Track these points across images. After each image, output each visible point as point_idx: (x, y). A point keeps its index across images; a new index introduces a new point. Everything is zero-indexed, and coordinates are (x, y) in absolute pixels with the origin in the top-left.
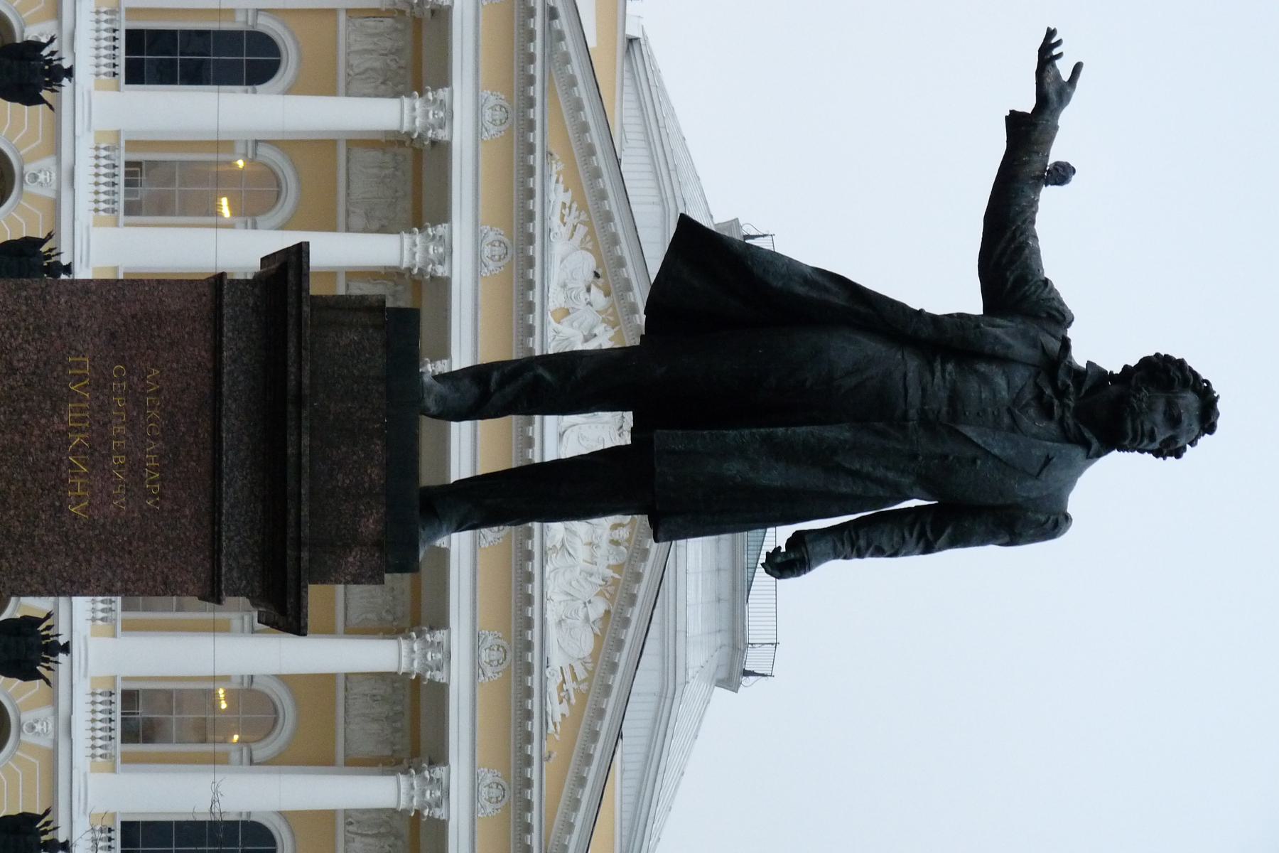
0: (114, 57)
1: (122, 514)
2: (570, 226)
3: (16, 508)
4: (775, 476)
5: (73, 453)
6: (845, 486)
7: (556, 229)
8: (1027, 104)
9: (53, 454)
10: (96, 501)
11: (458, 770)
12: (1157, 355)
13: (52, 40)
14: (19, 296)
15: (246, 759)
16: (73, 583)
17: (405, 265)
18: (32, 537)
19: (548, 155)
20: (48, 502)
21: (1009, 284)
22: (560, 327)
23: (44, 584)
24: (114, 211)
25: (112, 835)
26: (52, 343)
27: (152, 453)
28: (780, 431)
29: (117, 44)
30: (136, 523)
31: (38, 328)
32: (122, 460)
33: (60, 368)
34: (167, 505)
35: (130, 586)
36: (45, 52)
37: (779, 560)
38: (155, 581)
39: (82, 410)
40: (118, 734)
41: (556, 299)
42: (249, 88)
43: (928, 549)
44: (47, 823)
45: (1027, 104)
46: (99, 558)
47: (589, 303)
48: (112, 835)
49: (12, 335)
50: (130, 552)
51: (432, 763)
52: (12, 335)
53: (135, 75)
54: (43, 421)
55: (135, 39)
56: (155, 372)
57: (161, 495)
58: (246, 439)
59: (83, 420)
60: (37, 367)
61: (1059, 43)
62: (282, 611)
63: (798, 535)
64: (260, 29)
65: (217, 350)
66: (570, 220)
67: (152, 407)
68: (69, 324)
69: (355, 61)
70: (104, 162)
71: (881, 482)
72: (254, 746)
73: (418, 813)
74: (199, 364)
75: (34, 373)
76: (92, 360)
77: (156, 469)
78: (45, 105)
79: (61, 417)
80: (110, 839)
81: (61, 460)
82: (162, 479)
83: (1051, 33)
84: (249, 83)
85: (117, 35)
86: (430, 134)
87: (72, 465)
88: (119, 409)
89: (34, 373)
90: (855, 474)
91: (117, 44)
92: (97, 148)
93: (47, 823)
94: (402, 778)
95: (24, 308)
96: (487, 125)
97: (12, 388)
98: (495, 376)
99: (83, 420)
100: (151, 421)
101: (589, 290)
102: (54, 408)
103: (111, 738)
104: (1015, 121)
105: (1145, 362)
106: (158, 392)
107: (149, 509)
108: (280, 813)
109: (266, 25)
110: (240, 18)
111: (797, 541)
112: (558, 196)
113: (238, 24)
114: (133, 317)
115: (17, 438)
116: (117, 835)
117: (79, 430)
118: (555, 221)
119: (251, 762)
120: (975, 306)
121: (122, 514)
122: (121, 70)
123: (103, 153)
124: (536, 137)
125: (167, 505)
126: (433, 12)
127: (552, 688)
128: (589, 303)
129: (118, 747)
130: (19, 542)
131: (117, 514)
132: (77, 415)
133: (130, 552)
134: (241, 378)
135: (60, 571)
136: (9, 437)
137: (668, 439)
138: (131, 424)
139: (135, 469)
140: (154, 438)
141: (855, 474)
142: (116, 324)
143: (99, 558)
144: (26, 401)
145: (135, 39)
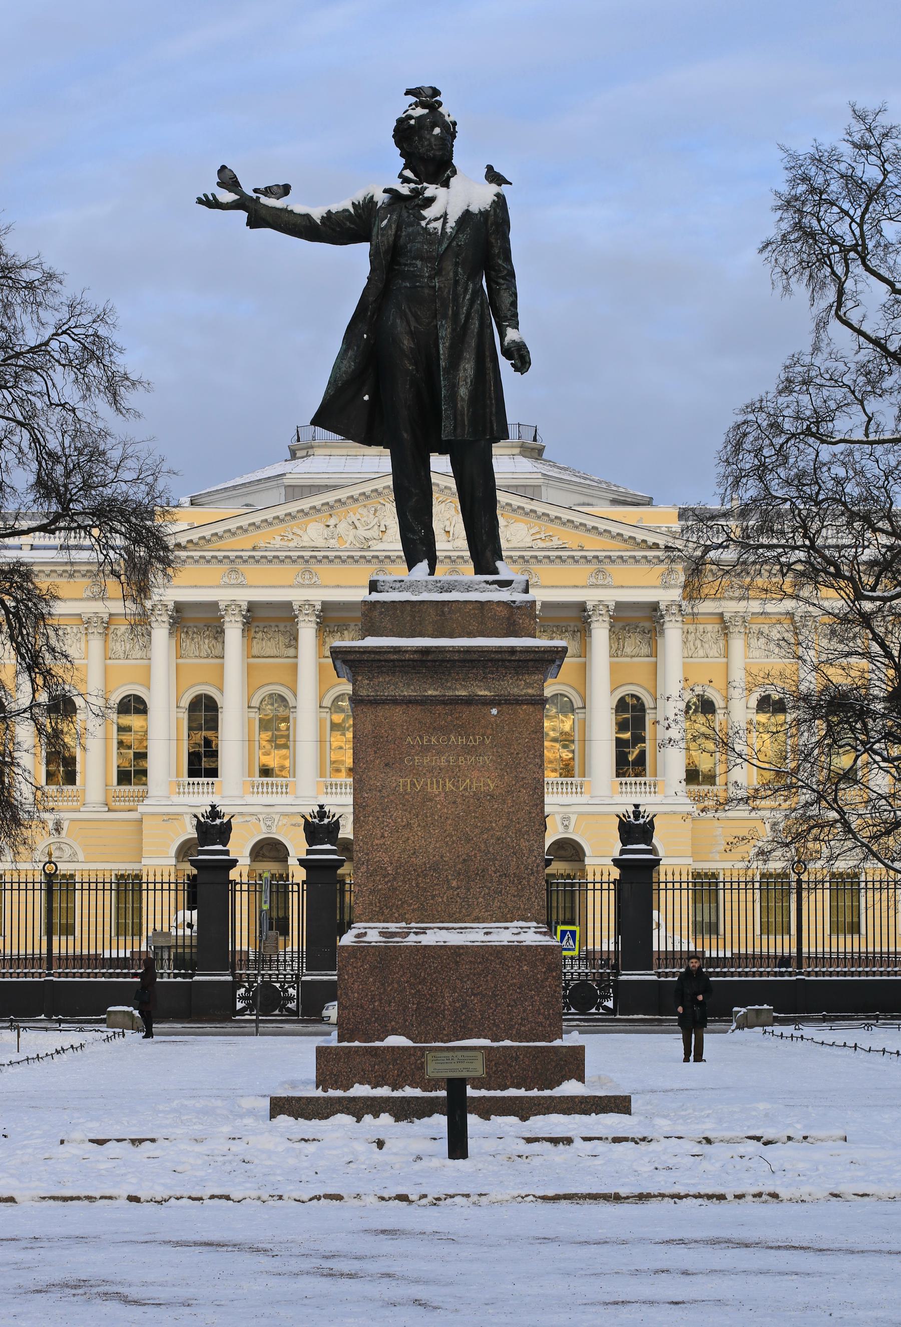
0: (203, 784)
1: (494, 758)
2: (294, 537)
3: (491, 822)
4: (468, 368)
5: (458, 788)
6: (475, 325)
7: (295, 544)
8: (243, 215)
9: (459, 800)
10: (487, 774)
11: (590, 596)
12: (393, 136)
13: (196, 816)
14: (363, 821)
15: (583, 711)
16: (536, 788)
17: (315, 626)
18: (509, 813)
19: (254, 549)
20: (487, 803)
21: (352, 226)
22: (349, 542)
23: (537, 805)
25: (624, 782)
26: (392, 801)
27: (457, 741)
28: (443, 364)
29: (196, 783)
31: (383, 810)
32: (461, 758)
33: (407, 797)
34: (489, 731)
35: (538, 754)
36: (202, 820)
37: (519, 365)
38: (534, 739)
39: (432, 783)
40: (569, 780)
42: (220, 710)
43: (512, 274)
44: (624, 816)
45: (243, 215)
46: (521, 772)
47: (335, 526)
48: (624, 782)
49: (387, 826)
50: (517, 754)
51: (585, 610)
52: (387, 826)
53: (213, 773)
54: (439, 806)
55: (193, 773)
56: (409, 739)
57: (483, 735)
58: (449, 684)
59: (438, 782)
60: (406, 810)
61: (205, 195)
62: (553, 661)
63: (504, 354)
64: (187, 706)
65: (395, 702)
66: (290, 537)
67: (430, 741)
68: (380, 791)
69: (204, 654)
71: (472, 302)
72: (575, 707)
73: (611, 617)
74: (404, 713)
75: (410, 812)
77: (467, 739)
78: (232, 820)
79: (436, 796)
80: (626, 784)
81: (463, 795)
82: (474, 735)
83: (200, 201)
84: (217, 711)
85: (191, 782)
86: (244, 613)
87: (465, 789)
88: (431, 761)
89: (410, 812)
90: (468, 316)
91: (196, 783)
92: (253, 793)
93: (624, 816)
94: (593, 626)
95: (371, 818)
97: (419, 825)
98: (378, 606)
99: (438, 782)
100: (438, 741)
101: (328, 526)
102: (431, 800)
103: (572, 784)
104: (253, 223)
105: (398, 144)
106: (421, 738)
107: (491, 742)
108: (612, 692)
109: (185, 702)
110: (181, 715)
111: (507, 354)
112: (277, 542)
113: (185, 716)
114: (375, 752)
115: (449, 822)
116: (624, 780)
117: (444, 785)
118: (292, 544)
119: (584, 708)
120: (364, 248)
121: (494, 758)
122: (210, 780)
123: (255, 790)
124: (245, 554)
125: (489, 731)
127: (541, 544)
128: (335, 526)
129: (576, 780)
130: (511, 820)
131: (494, 762)
132: (435, 786)
133: (517, 754)
134: (412, 687)
135: (529, 796)
136: (448, 827)
137: (446, 432)
138: (440, 753)
140: (449, 739)
141: (468, 316)
142: (379, 764)
143: (521, 772)
144: (427, 817)
145: (193, 773)
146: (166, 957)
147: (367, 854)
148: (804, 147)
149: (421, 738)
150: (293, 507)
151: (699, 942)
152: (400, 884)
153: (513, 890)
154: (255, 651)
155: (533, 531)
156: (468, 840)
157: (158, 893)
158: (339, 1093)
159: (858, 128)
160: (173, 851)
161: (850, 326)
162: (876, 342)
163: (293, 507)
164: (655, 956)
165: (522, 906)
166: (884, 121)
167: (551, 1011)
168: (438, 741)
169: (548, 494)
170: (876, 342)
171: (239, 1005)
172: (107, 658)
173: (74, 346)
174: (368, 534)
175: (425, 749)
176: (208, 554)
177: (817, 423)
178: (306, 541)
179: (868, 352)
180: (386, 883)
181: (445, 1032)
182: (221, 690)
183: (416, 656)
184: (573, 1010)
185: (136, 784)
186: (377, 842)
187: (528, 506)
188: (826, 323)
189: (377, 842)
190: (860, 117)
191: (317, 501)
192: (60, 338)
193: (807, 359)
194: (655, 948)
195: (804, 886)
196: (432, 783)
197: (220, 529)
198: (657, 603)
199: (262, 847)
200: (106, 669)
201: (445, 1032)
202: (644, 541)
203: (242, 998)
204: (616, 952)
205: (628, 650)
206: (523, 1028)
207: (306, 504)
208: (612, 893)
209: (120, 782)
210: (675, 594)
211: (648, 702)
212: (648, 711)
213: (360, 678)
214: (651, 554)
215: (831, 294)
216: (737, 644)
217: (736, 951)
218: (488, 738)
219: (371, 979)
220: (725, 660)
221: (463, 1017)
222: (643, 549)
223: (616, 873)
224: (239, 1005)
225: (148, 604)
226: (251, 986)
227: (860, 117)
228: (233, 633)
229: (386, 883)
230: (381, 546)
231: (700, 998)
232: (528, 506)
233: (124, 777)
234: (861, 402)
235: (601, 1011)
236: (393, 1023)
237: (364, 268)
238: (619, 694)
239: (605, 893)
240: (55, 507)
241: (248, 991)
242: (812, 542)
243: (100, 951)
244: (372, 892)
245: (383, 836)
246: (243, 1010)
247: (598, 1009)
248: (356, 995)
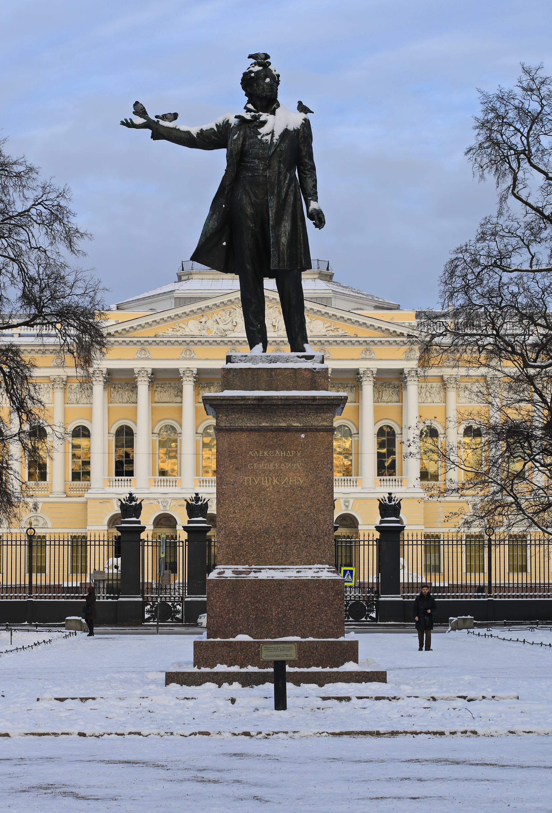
0: (124, 480)
1: (303, 465)
2: (180, 329)
3: (301, 504)
4: (286, 226)
5: (280, 483)
6: (291, 199)
7: (181, 333)
8: (149, 132)
9: (281, 490)
10: (298, 474)
11: (362, 365)
12: (241, 84)
13: (120, 500)
15: (357, 435)
16: (328, 483)
17: (193, 384)
18: (312, 498)
19: (156, 336)
20: (299, 492)
21: (216, 139)
22: (214, 332)
24: (176, 481)
25: (382, 479)
26: (240, 491)
27: (280, 454)
28: (271, 223)
29: (120, 479)
30: (306, 460)
31: (234, 496)
32: (283, 465)
33: (249, 488)
34: (300, 448)
37: (318, 223)
38: (327, 453)
39: (265, 480)
40: (349, 478)
41: (204, 332)
42: (135, 435)
43: (314, 168)
44: (382, 500)
45: (149, 132)
46: (319, 473)
47: (205, 322)
48: (382, 479)
49: (237, 506)
50: (317, 462)
52: (237, 506)
53: (130, 473)
54: (269, 494)
55: (118, 474)
56: (251, 453)
57: (296, 451)
58: (275, 419)
59: (268, 479)
60: (249, 496)
61: (126, 120)
62: (339, 405)
63: (309, 217)
64: (115, 432)
65: (242, 430)
67: (263, 454)
68: (233, 485)
69: (125, 401)
70: (159, 484)
71: (289, 185)
72: (352, 433)
73: (374, 378)
75: (251, 498)
76: (246, 476)
77: (286, 452)
78: (142, 502)
79: (267, 488)
80: (384, 480)
81: (283, 487)
82: (290, 450)
83: (123, 123)
84: (133, 435)
85: (117, 479)
86: (149, 376)
87: (285, 484)
88: (264, 466)
89: (251, 498)
91: (120, 479)
92: (155, 486)
93: (382, 500)
94: (363, 383)
96: (146, 356)
97: (257, 506)
99: (268, 479)
100: (268, 454)
101: (201, 322)
102: (264, 490)
103: (350, 480)
104: (155, 136)
105: (244, 88)
108: (375, 424)
109: (114, 430)
110: (111, 438)
112: (170, 332)
113: (114, 439)
114: (230, 461)
115: (275, 503)
116: (382, 478)
117: (272, 481)
118: (179, 334)
119: (358, 434)
120: (223, 152)
121: (303, 465)
122: (129, 478)
123: (156, 484)
125: (300, 448)
126: (109, 375)
127: (332, 333)
128: (205, 322)
129: (353, 478)
130: (313, 503)
132: (266, 482)
133: (317, 462)
134: (252, 421)
135: (324, 487)
137: (273, 265)
138: (269, 461)
139: (287, 460)
140: (275, 453)
141: (287, 194)
142: (232, 468)
143: (319, 473)
144: (261, 500)
145: (118, 474)
146: (102, 586)
147: (225, 523)
148: (492, 90)
149: (258, 452)
150: (180, 311)
151: (428, 577)
152: (245, 541)
153: (314, 546)
154: (156, 399)
155: (326, 325)
156: (287, 515)
157: (97, 547)
158: (208, 670)
159: (526, 78)
160: (106, 522)
161: (521, 200)
162: (537, 210)
163: (180, 311)
164: (402, 586)
165: (320, 555)
166: (542, 74)
167: (338, 620)
168: (268, 454)
169: (336, 303)
170: (537, 210)
171: (147, 616)
172: (65, 403)
173: (45, 212)
174: (226, 327)
175: (261, 459)
176: (128, 340)
177: (501, 259)
178: (187, 332)
179: (532, 216)
180: (237, 541)
181: (273, 632)
182: (136, 423)
183: (255, 402)
184: (351, 619)
185: (83, 480)
186: (231, 516)
187: (324, 310)
188: (506, 198)
189: (231, 516)
190: (527, 71)
191: (194, 307)
192: (37, 207)
193: (494, 220)
194: (401, 581)
195: (493, 543)
196: (265, 480)
197: (135, 324)
198: (403, 370)
199: (161, 519)
200: (65, 410)
201: (273, 632)
202: (395, 332)
203: (148, 612)
204: (377, 583)
205: (385, 398)
206: (320, 630)
207: (187, 309)
208: (375, 547)
209: (73, 479)
210: (414, 364)
211: (397, 430)
212: (397, 436)
213: (220, 416)
214: (399, 339)
215: (509, 180)
216: (452, 394)
217: (451, 582)
218: (299, 452)
219: (227, 600)
220: (444, 404)
221: (284, 623)
222: (394, 336)
223: (377, 535)
224: (147, 616)
225: (91, 370)
226: (154, 604)
227: (527, 71)
228: (143, 388)
229: (237, 541)
230: (233, 335)
231: (429, 611)
232: (324, 310)
233: (76, 476)
234: (528, 247)
235: (368, 619)
236: (241, 627)
237: (223, 164)
238: (379, 425)
239: (371, 547)
240: (33, 311)
241: (152, 607)
242: (498, 332)
243: (61, 583)
244: (228, 546)
245: (234, 512)
246: (149, 619)
247: (366, 618)
248: (218, 610)
